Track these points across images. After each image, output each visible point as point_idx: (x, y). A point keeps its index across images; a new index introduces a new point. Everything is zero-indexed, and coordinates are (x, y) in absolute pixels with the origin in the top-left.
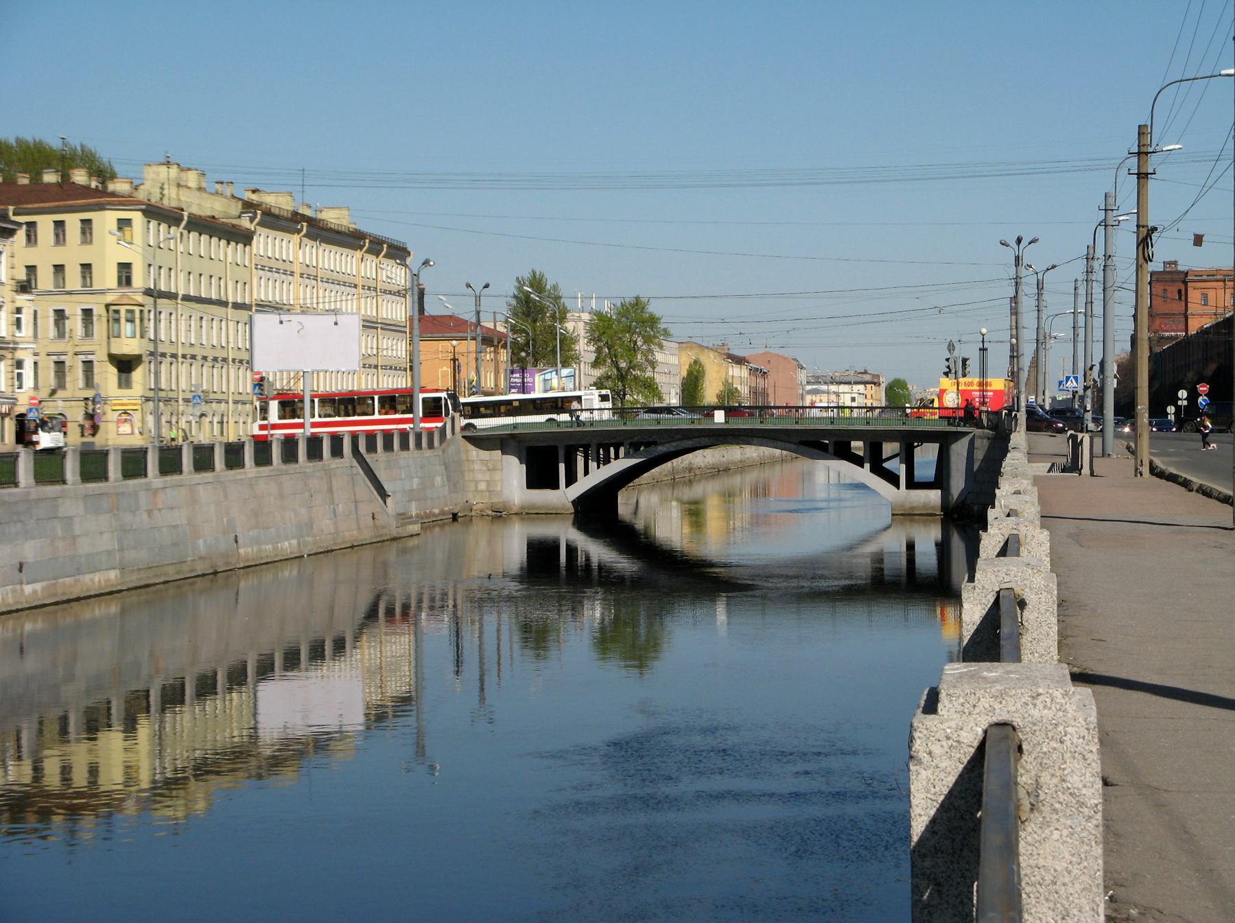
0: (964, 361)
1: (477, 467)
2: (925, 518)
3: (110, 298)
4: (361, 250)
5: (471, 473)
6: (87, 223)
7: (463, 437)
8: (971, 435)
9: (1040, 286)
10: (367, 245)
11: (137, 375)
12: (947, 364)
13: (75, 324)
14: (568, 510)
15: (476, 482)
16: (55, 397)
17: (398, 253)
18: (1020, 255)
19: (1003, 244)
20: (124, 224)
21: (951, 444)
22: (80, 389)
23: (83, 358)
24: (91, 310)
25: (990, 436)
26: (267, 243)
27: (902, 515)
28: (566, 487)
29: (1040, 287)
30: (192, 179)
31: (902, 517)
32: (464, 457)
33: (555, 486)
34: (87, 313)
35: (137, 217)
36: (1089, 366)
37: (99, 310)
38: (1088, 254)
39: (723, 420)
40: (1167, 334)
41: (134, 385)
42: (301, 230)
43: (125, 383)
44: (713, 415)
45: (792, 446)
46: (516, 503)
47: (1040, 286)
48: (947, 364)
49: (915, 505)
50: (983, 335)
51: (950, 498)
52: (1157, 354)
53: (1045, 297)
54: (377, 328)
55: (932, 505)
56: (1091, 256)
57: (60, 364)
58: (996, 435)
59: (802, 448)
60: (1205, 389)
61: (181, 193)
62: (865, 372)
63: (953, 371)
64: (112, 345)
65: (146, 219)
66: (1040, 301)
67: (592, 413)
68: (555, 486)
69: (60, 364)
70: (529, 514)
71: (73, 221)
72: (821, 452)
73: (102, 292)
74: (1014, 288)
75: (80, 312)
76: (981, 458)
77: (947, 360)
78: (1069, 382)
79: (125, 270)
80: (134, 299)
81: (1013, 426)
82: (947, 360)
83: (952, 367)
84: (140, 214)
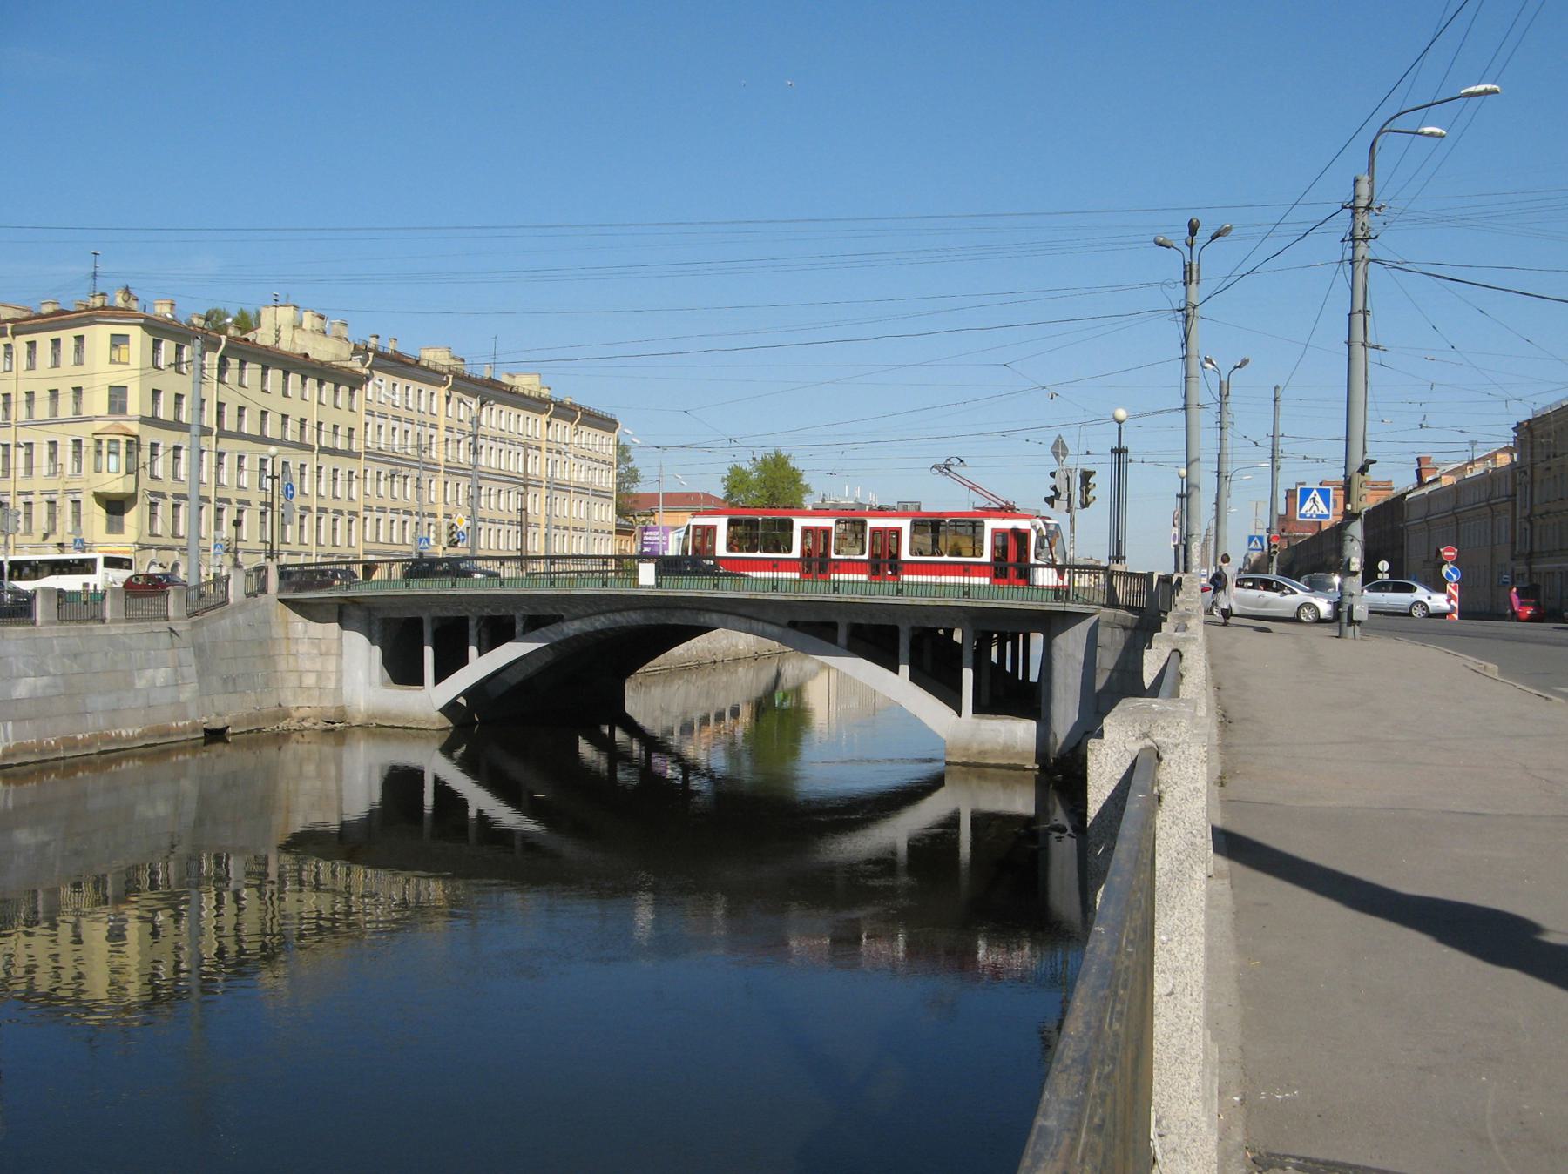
0: (1086, 476)
1: (303, 648)
2: (1004, 771)
3: (99, 426)
4: (547, 414)
5: (291, 659)
6: (80, 339)
7: (280, 600)
8: (1096, 617)
9: (1223, 394)
10: (552, 409)
11: (131, 518)
12: (1052, 481)
13: (66, 454)
14: (434, 723)
15: (301, 673)
16: (46, 542)
17: (606, 423)
18: (1195, 263)
19: (1161, 245)
20: (118, 341)
21: (1055, 637)
22: (69, 533)
23: (71, 497)
24: (80, 441)
25: (1129, 624)
26: (382, 388)
27: (964, 764)
28: (436, 683)
29: (1225, 392)
30: (308, 320)
31: (964, 769)
32: (278, 632)
33: (418, 680)
34: (78, 443)
35: (136, 333)
36: (1357, 461)
37: (88, 443)
38: (1356, 197)
39: (652, 581)
40: (1298, 534)
41: (126, 529)
42: (447, 382)
43: (115, 527)
44: (636, 571)
45: (776, 630)
46: (362, 708)
47: (1223, 394)
48: (1052, 481)
49: (988, 746)
50: (1120, 422)
51: (1051, 739)
52: (1293, 546)
53: (1231, 407)
54: (569, 491)
55: (1019, 748)
56: (1363, 202)
57: (52, 503)
58: (1140, 621)
59: (792, 632)
60: (1453, 554)
61: (296, 335)
62: (1091, 559)
63: (1064, 496)
64: (201, 491)
65: (151, 338)
66: (1225, 414)
67: (502, 564)
68: (693, 526)
69: (52, 503)
70: (382, 729)
71: (67, 336)
72: (825, 644)
73: (90, 419)
74: (1181, 326)
75: (71, 443)
76: (1111, 666)
77: (1053, 474)
78: (1308, 504)
79: (117, 396)
80: (123, 428)
81: (444, 874)
82: (1053, 474)
83: (1062, 487)
84: (139, 329)
